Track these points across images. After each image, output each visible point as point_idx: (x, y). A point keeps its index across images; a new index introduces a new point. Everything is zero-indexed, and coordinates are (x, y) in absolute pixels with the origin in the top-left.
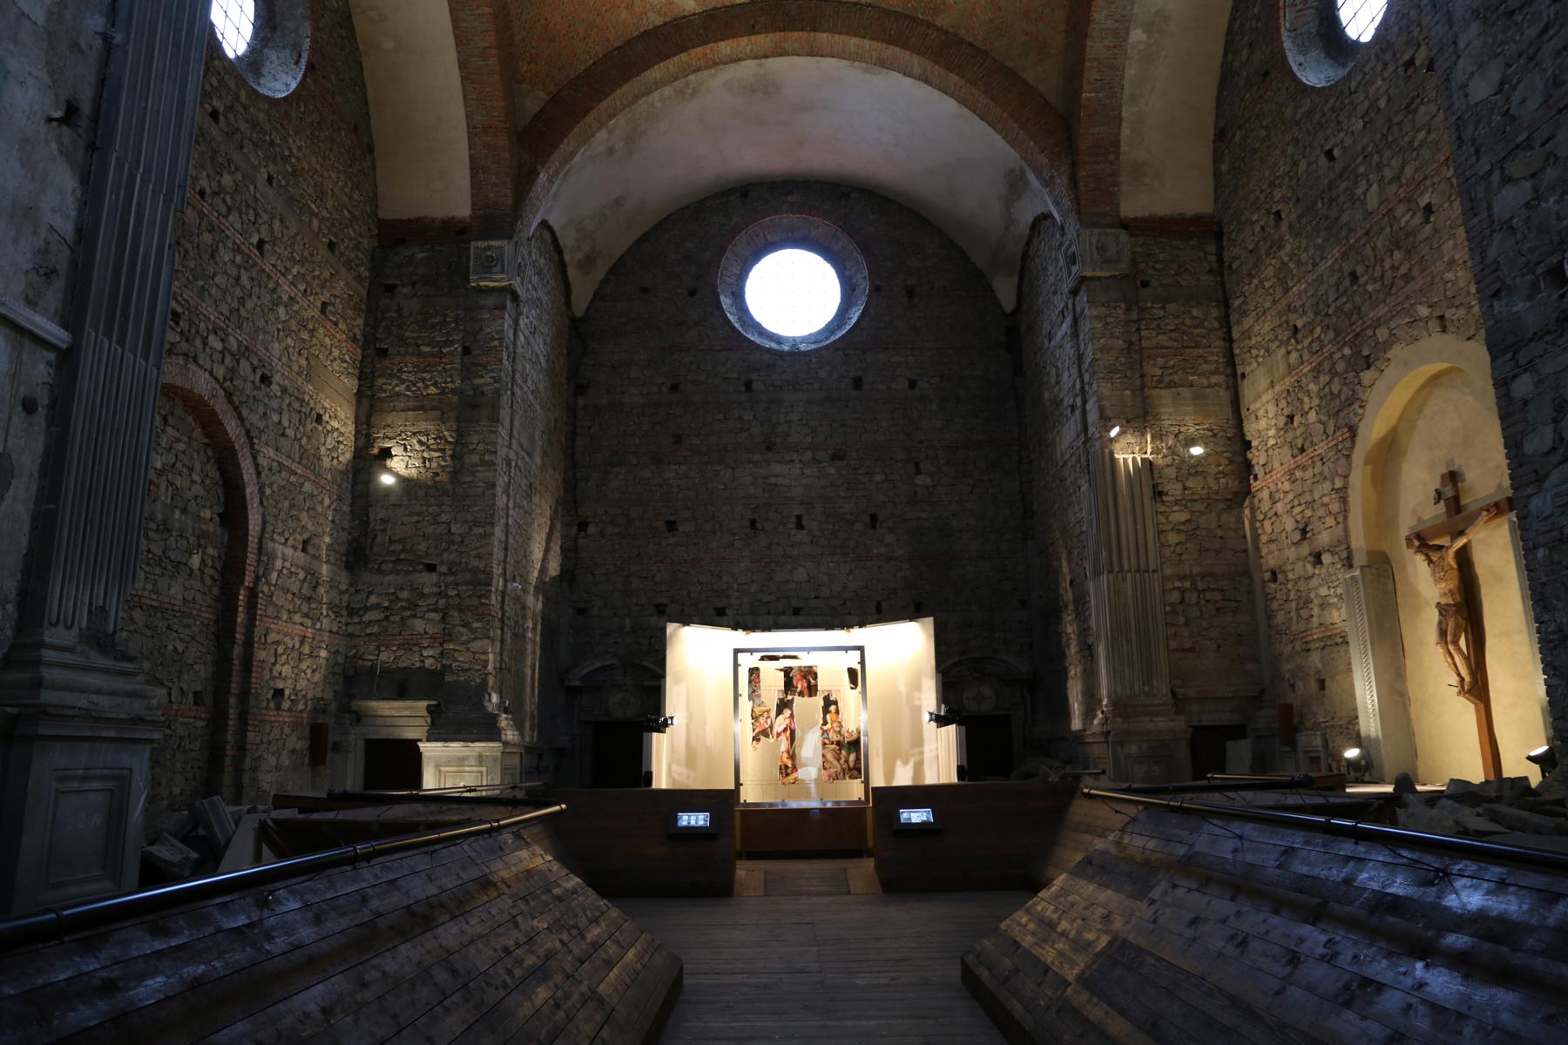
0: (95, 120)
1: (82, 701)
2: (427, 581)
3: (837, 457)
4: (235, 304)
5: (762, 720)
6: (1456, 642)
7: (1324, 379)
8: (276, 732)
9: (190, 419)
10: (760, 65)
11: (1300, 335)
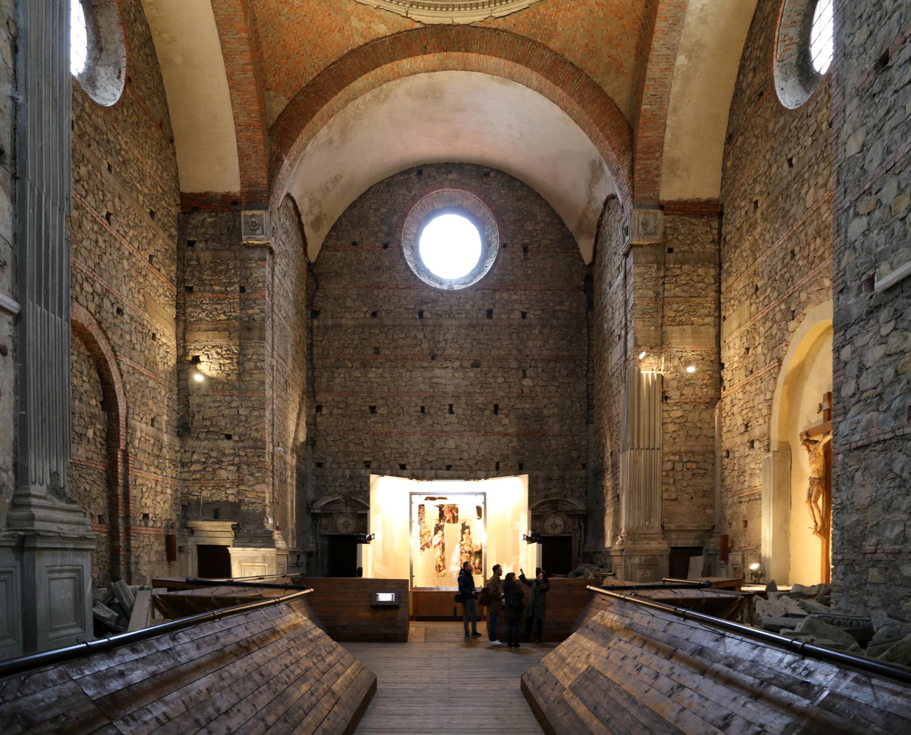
0: (14, 158)
1: (54, 527)
2: (227, 445)
3: (476, 365)
4: (97, 260)
5: (426, 537)
6: (816, 502)
7: (768, 324)
8: (147, 540)
9: (77, 339)
10: (430, 77)
11: (758, 293)
